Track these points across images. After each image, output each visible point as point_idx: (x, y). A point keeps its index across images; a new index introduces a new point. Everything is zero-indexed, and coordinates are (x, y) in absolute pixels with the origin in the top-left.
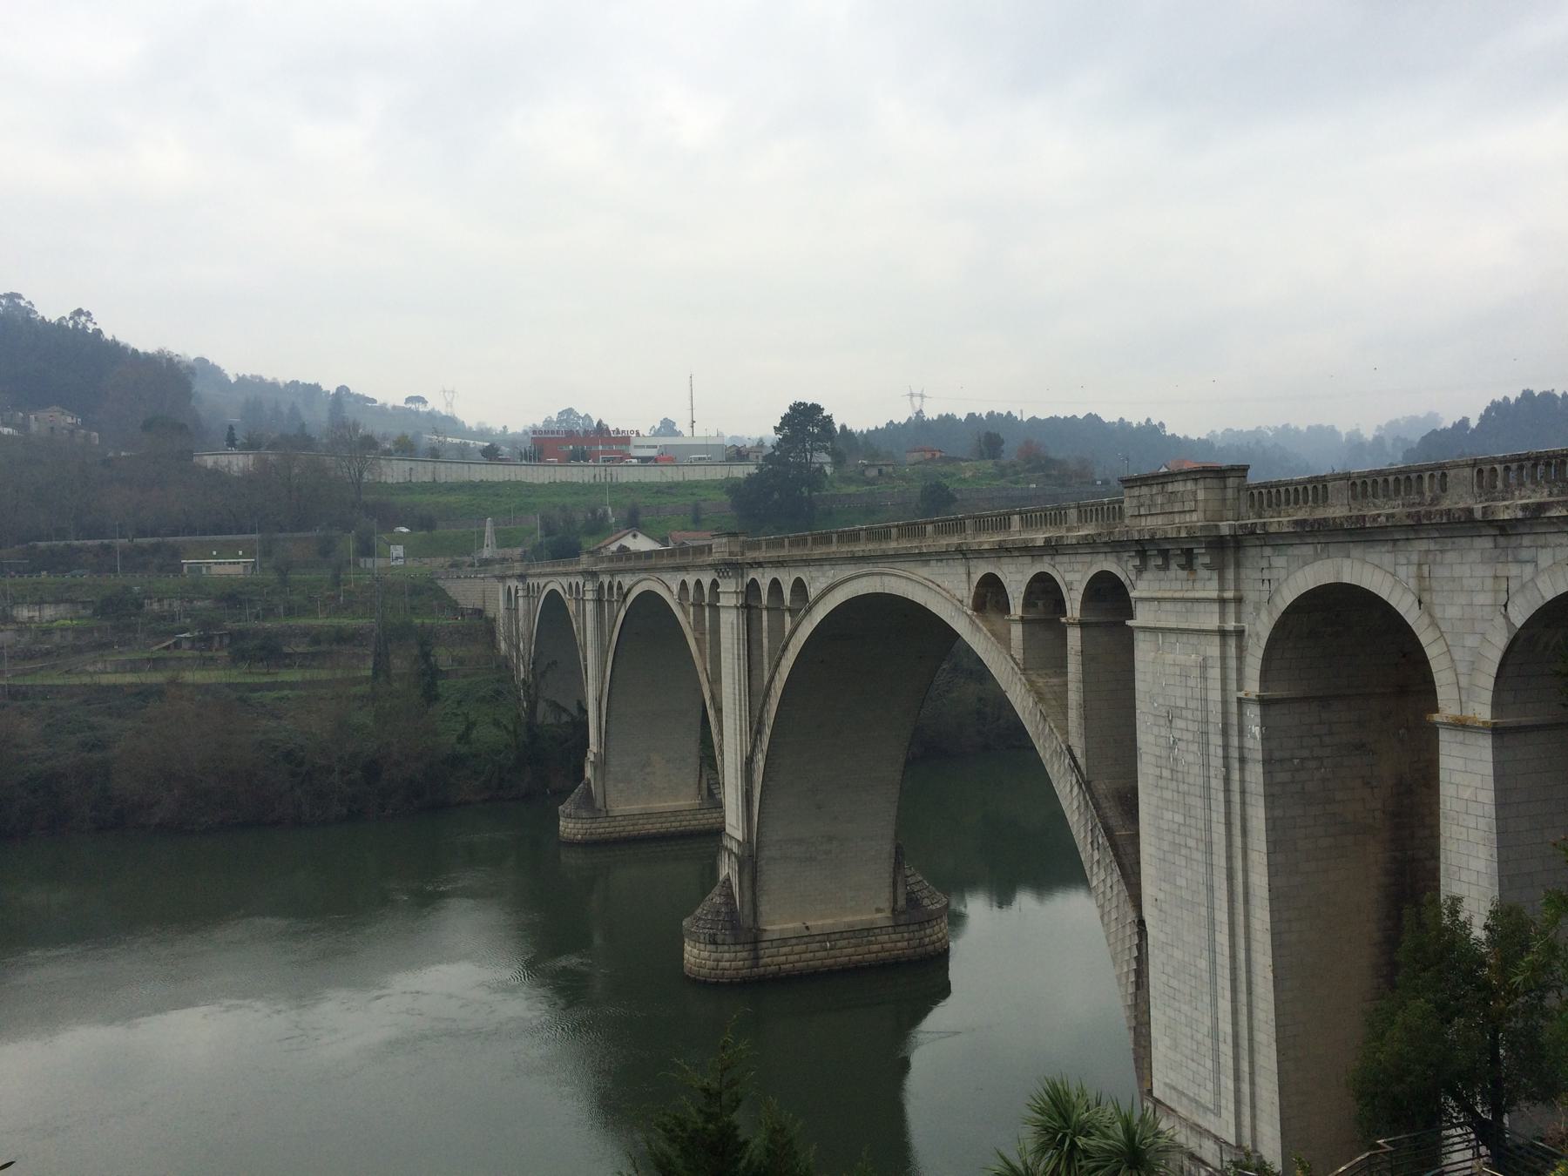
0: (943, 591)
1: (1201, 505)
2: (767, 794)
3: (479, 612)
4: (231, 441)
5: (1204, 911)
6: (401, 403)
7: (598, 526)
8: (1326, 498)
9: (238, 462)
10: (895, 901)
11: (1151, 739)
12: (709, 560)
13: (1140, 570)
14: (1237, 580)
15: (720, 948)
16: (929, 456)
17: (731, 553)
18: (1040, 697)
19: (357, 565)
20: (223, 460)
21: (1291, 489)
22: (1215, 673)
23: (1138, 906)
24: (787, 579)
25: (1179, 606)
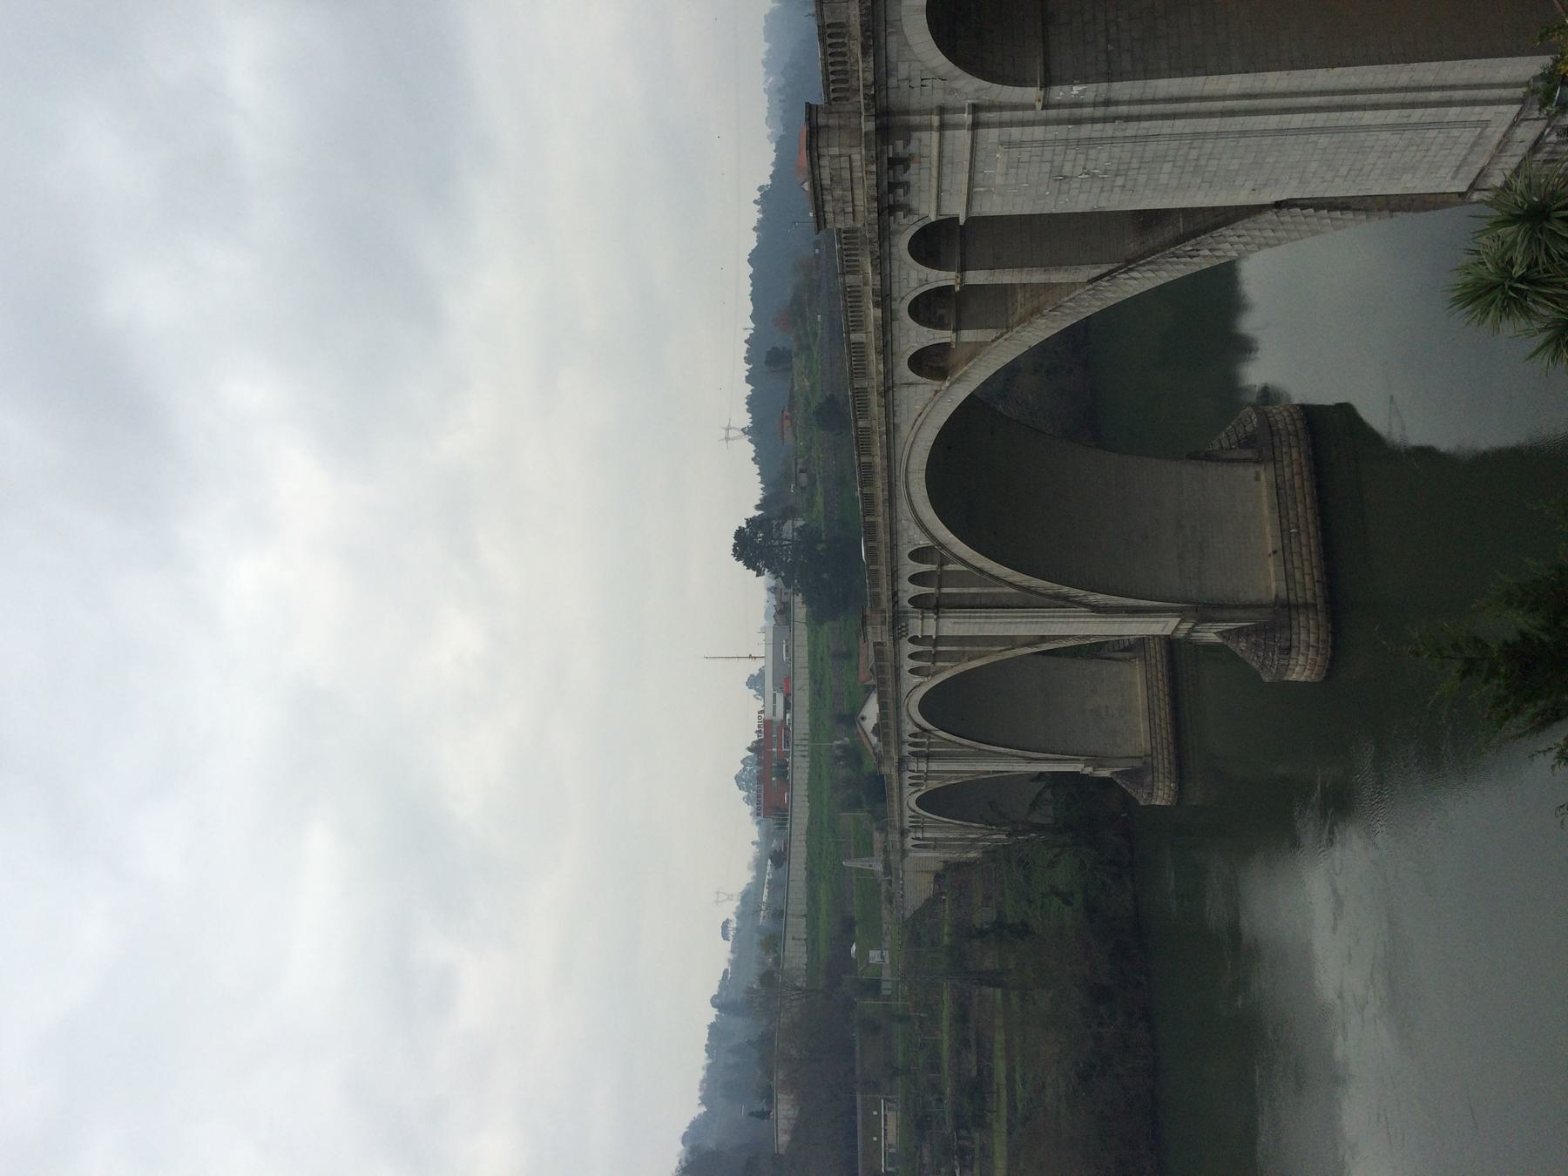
0: (926, 410)
1: (844, 151)
3: (938, 877)
5: (1268, 141)
6: (728, 945)
7: (853, 755)
9: (785, 1109)
10: (1245, 460)
11: (1083, 197)
12: (889, 645)
13: (909, 210)
14: (920, 112)
15: (1295, 643)
16: (787, 423)
17: (883, 623)
19: (888, 998)
20: (783, 1124)
21: (830, 60)
22: (1016, 133)
23: (1261, 208)
24: (910, 567)
25: (946, 170)
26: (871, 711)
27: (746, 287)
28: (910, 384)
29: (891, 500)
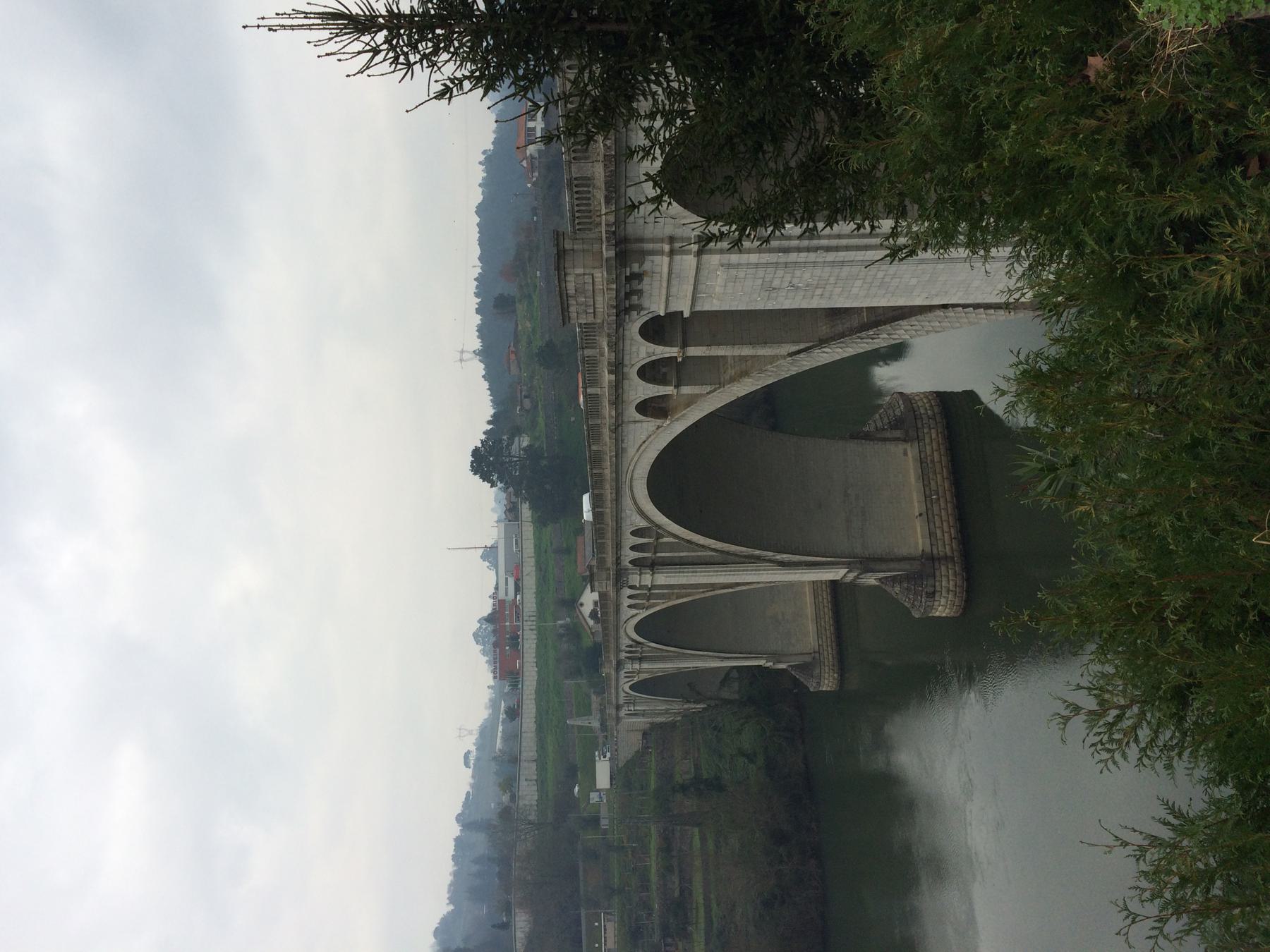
0: (648, 441)
1: (587, 271)
2: (813, 553)
3: (645, 734)
4: (505, 926)
6: (470, 771)
7: (574, 632)
8: (589, 179)
9: (522, 923)
12: (612, 594)
13: (639, 308)
14: (653, 240)
15: (938, 589)
16: (513, 357)
17: (608, 579)
18: (745, 374)
19: (605, 832)
20: (519, 935)
21: (576, 202)
23: (931, 308)
25: (674, 282)
26: (589, 599)
27: (474, 234)
28: (635, 422)
29: (618, 499)
